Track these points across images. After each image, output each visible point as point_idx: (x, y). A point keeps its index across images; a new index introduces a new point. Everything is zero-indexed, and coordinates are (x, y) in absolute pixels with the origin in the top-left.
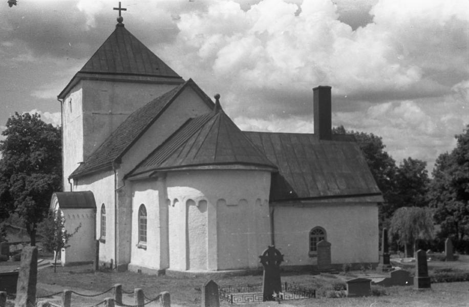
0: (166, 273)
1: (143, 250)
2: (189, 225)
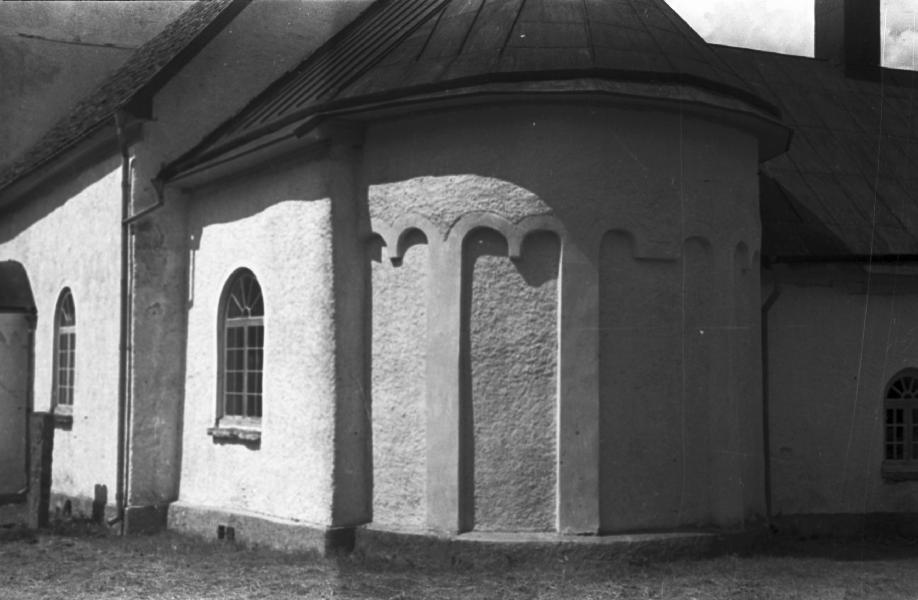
0: (361, 544)
1: (241, 449)
2: (475, 339)
